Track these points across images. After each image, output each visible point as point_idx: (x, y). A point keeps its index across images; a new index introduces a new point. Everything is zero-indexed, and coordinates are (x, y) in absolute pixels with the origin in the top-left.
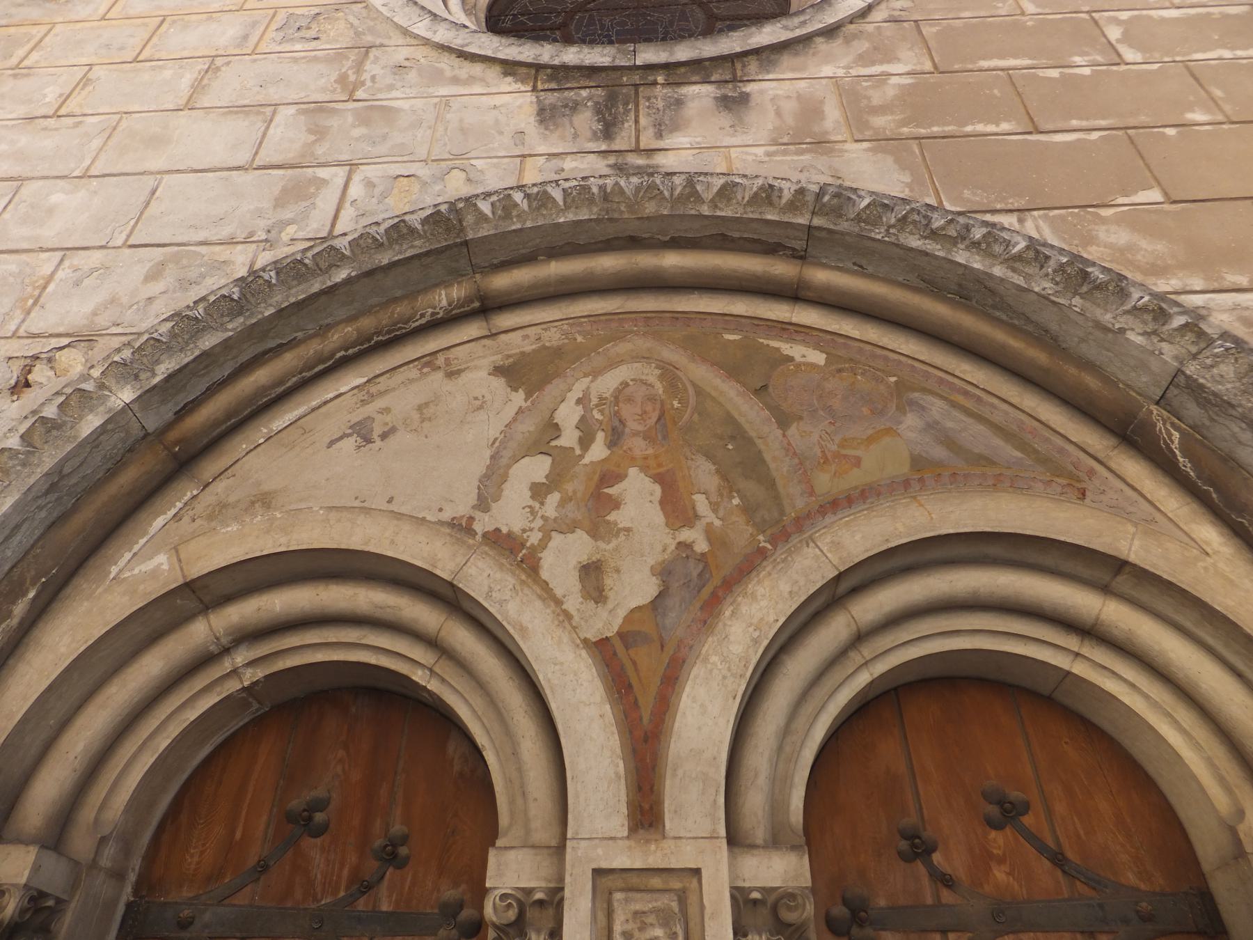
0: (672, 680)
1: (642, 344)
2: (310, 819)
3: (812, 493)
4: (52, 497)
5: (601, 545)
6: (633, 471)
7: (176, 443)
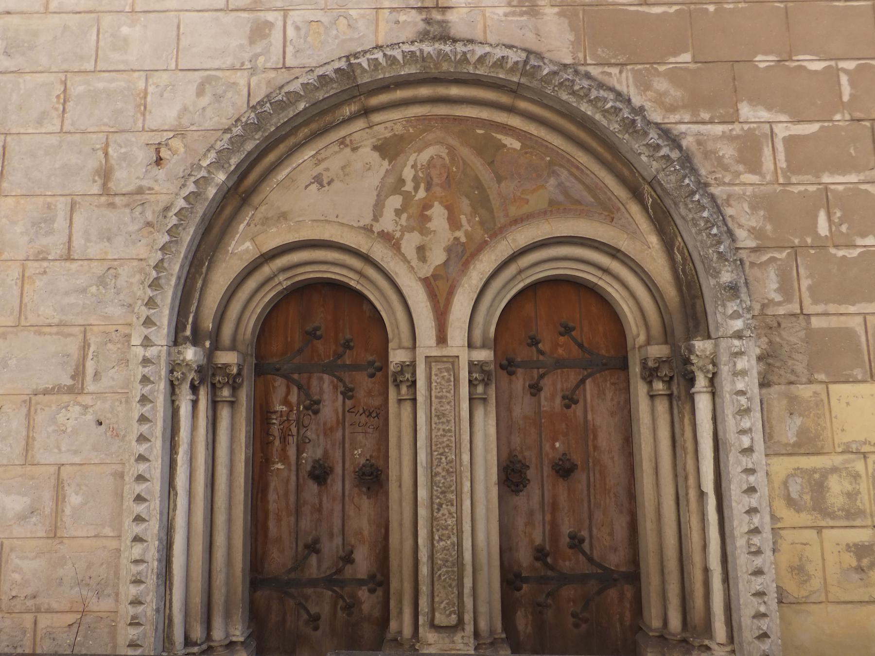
0: (451, 293)
1: (439, 134)
3: (507, 216)
6: (436, 203)
7: (243, 193)
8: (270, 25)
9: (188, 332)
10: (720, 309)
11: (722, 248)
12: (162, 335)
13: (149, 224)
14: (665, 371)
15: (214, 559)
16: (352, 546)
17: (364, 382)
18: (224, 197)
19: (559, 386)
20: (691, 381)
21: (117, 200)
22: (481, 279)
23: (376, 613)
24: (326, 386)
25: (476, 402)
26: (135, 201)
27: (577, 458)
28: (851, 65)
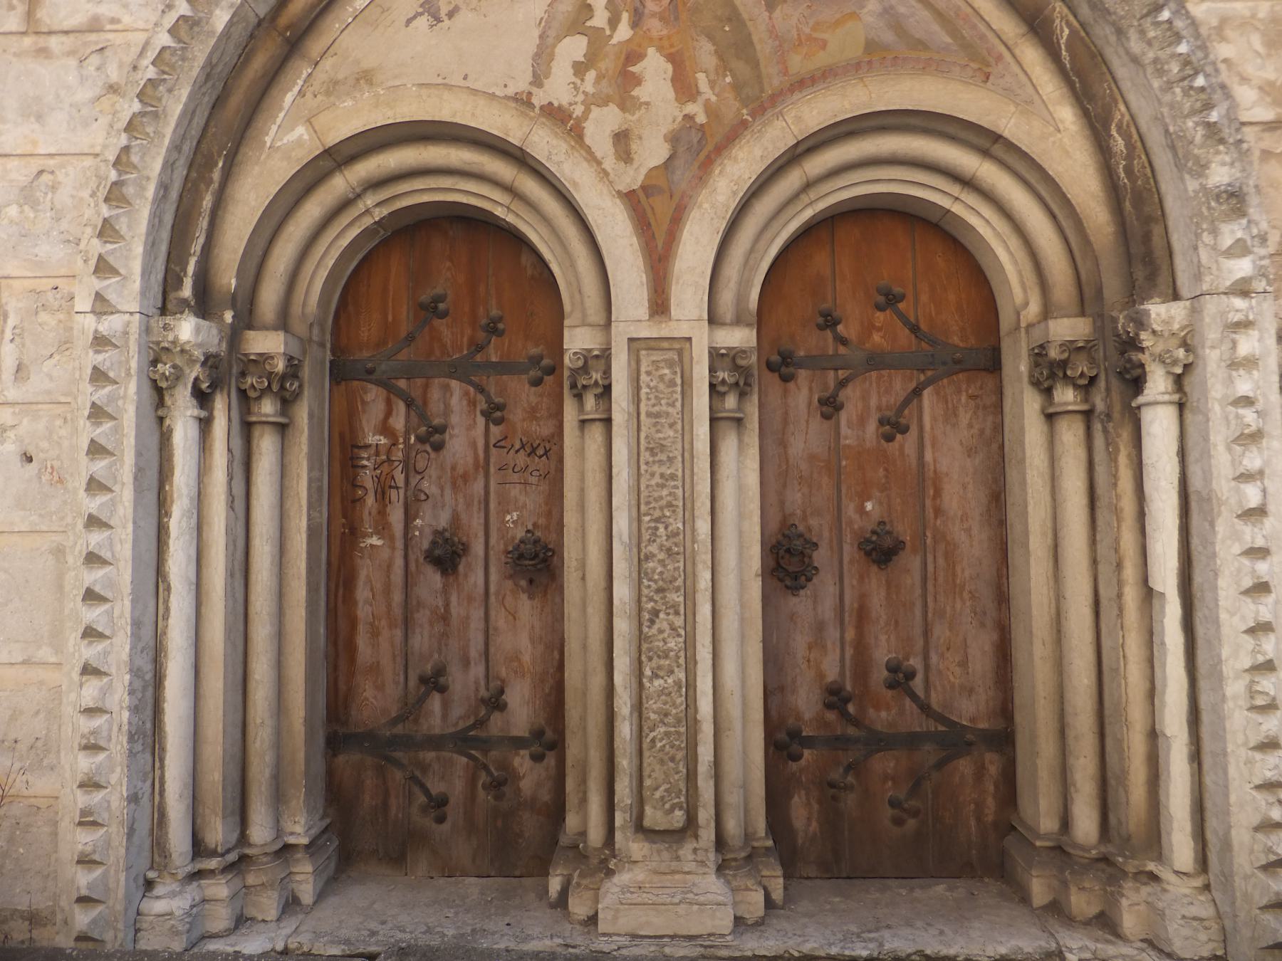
2: (436, 307)
3: (785, 72)
4: (209, 84)
5: (627, 115)
6: (651, 51)
7: (288, 28)
9: (187, 291)
10: (1207, 238)
11: (1214, 116)
12: (130, 293)
14: (1081, 367)
15: (250, 704)
16: (503, 681)
17: (521, 394)
18: (252, 36)
19: (873, 402)
20: (1136, 383)
21: (54, 42)
22: (735, 193)
23: (545, 796)
24: (456, 401)
25: (722, 424)
26: (85, 44)
27: (904, 530)
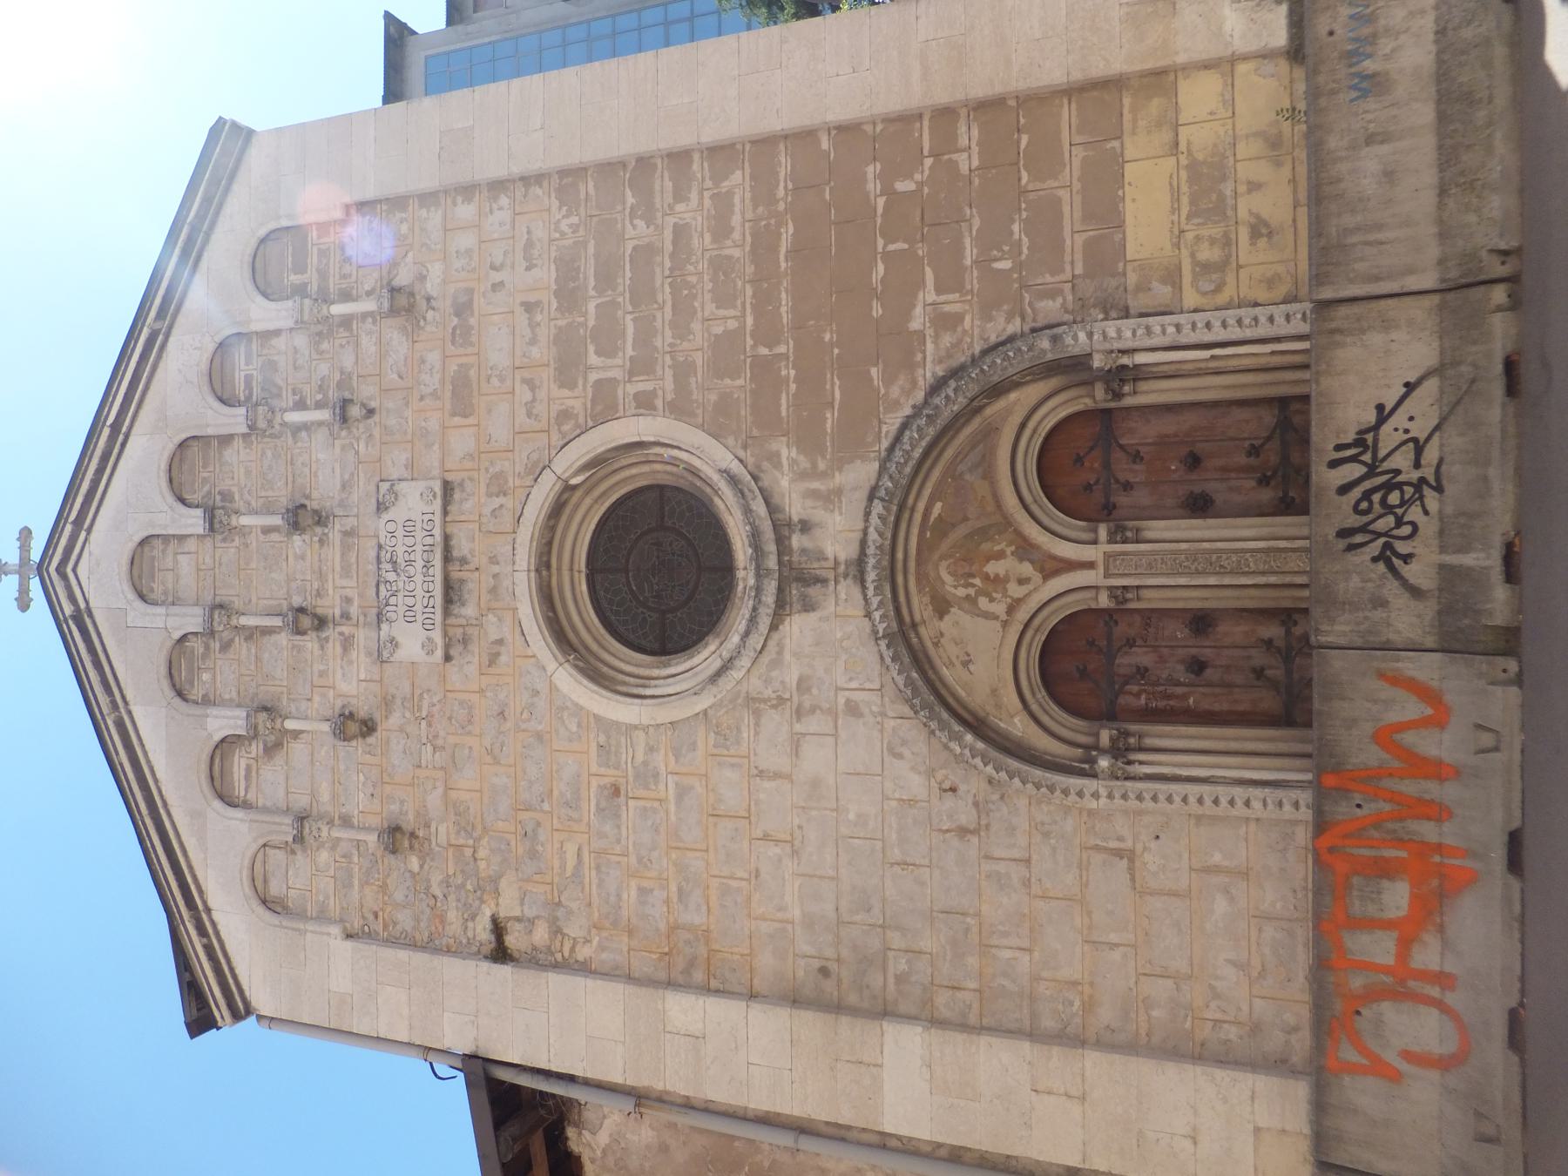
8: (848, 701)
12: (1089, 785)
13: (1002, 797)
17: (1121, 630)
20: (1124, 367)
21: (983, 822)
28: (880, 242)
